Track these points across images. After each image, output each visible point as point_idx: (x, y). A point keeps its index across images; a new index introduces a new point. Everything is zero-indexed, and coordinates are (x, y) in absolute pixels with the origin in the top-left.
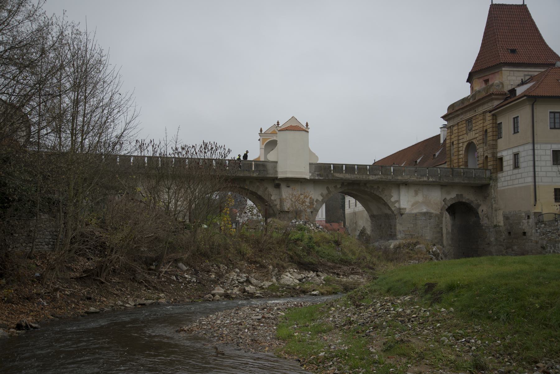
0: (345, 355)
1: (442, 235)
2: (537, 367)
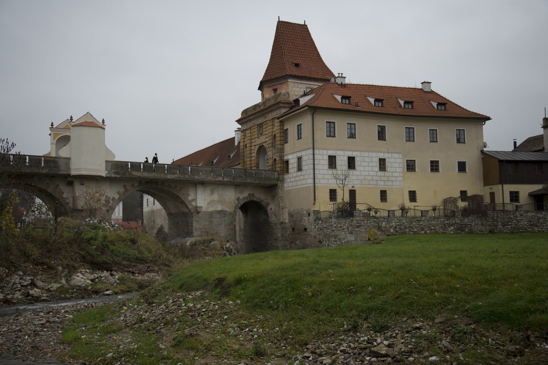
0: (134, 354)
1: (235, 231)
2: (307, 349)
